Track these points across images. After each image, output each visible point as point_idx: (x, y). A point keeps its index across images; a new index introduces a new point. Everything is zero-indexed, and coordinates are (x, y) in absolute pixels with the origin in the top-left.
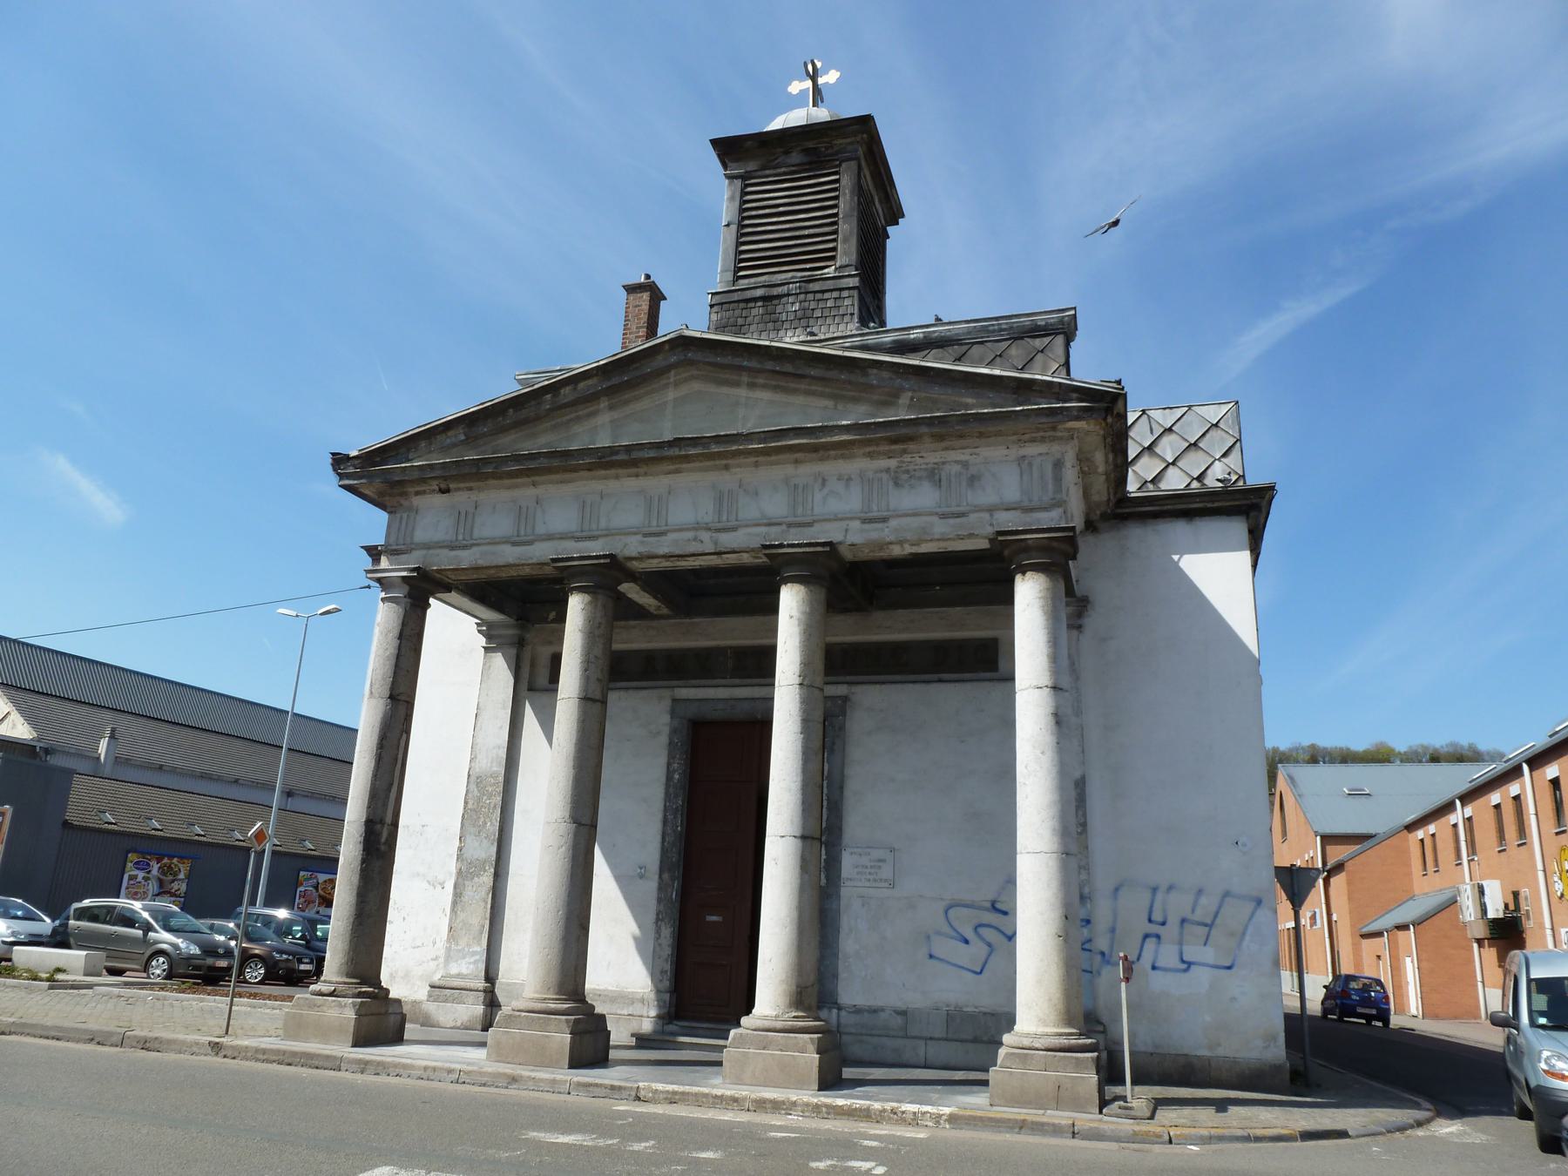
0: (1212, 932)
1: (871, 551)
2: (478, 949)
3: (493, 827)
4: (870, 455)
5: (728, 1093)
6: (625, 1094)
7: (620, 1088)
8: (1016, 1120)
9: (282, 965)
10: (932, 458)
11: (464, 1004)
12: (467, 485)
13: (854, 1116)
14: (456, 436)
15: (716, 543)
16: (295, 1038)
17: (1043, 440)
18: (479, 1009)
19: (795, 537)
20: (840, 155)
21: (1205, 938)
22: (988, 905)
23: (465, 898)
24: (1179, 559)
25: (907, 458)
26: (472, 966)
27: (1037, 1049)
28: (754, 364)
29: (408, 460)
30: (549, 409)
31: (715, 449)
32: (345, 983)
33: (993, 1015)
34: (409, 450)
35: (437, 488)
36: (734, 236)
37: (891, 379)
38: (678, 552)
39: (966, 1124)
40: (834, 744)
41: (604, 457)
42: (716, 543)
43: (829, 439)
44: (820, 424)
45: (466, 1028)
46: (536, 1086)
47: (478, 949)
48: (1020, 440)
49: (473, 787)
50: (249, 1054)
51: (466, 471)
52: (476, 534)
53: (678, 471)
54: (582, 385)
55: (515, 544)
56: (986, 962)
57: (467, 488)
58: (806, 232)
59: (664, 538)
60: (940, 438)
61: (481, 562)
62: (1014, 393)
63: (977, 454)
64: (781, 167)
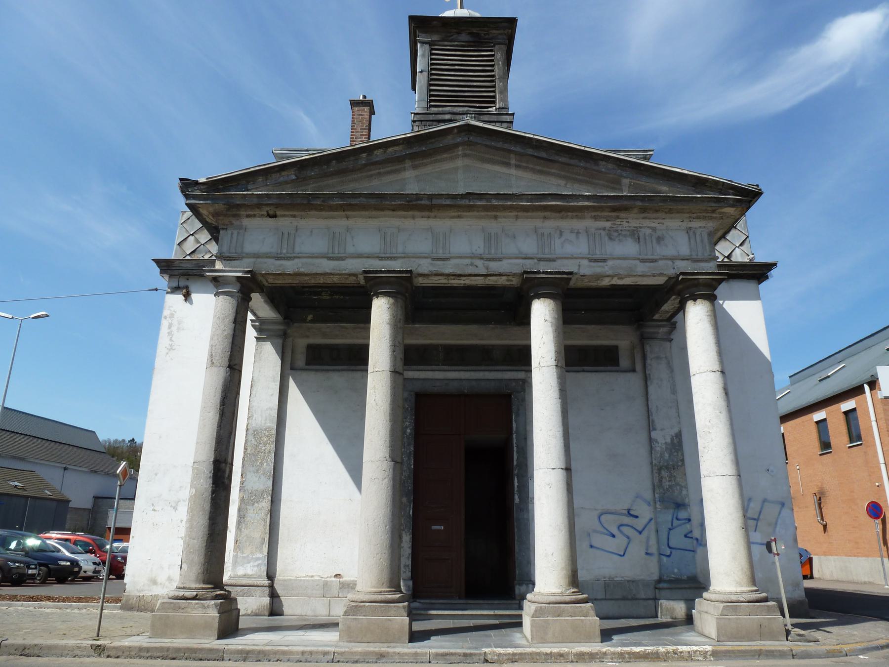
0: (759, 524)
1: (589, 281)
2: (261, 556)
3: (269, 466)
4: (596, 218)
5: (555, 650)
6: (475, 658)
7: (471, 655)
8: (755, 651)
9: (14, 571)
10: (634, 223)
11: (253, 597)
12: (291, 213)
13: (648, 658)
14: (288, 176)
15: (487, 268)
16: (163, 635)
17: (704, 218)
18: (267, 600)
19: (544, 267)
20: (494, 40)
21: (755, 527)
22: (626, 512)
23: (248, 519)
24: (723, 303)
25: (618, 222)
26: (255, 569)
27: (742, 602)
28: (518, 149)
29: (248, 190)
30: (364, 164)
31: (495, 203)
32: (203, 589)
33: (633, 581)
34: (248, 183)
35: (265, 213)
36: (426, 79)
37: (613, 169)
38: (459, 272)
39: (724, 656)
40: (518, 410)
41: (411, 201)
42: (487, 268)
43: (576, 204)
44: (571, 193)
45: (256, 615)
46: (400, 659)
47: (261, 556)
48: (690, 217)
49: (251, 437)
50: (133, 653)
51: (298, 202)
52: (297, 249)
53: (459, 217)
54: (390, 150)
55: (330, 259)
56: (627, 548)
58: (475, 84)
59: (448, 262)
60: (643, 210)
61: (302, 270)
62: (693, 187)
63: (663, 224)
64: (454, 42)
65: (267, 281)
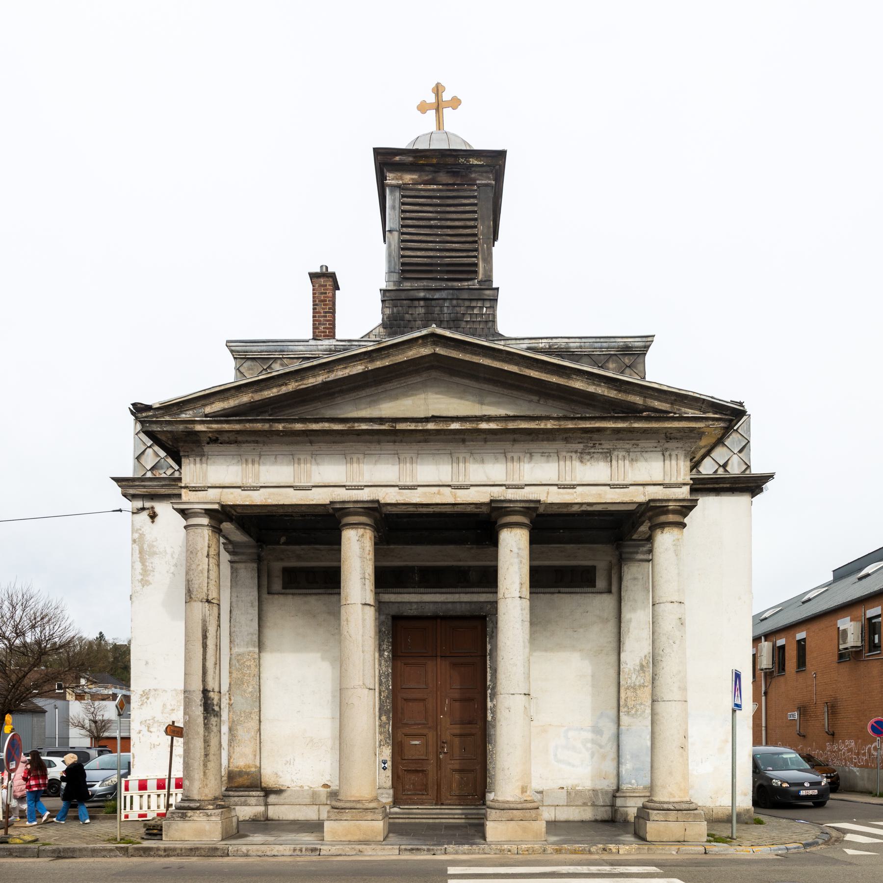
1: (558, 508)
57: (253, 441)
65: (235, 511)
